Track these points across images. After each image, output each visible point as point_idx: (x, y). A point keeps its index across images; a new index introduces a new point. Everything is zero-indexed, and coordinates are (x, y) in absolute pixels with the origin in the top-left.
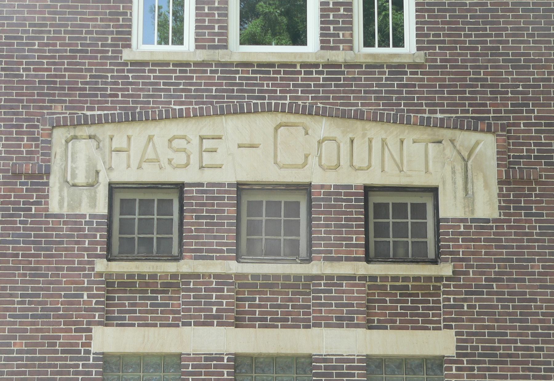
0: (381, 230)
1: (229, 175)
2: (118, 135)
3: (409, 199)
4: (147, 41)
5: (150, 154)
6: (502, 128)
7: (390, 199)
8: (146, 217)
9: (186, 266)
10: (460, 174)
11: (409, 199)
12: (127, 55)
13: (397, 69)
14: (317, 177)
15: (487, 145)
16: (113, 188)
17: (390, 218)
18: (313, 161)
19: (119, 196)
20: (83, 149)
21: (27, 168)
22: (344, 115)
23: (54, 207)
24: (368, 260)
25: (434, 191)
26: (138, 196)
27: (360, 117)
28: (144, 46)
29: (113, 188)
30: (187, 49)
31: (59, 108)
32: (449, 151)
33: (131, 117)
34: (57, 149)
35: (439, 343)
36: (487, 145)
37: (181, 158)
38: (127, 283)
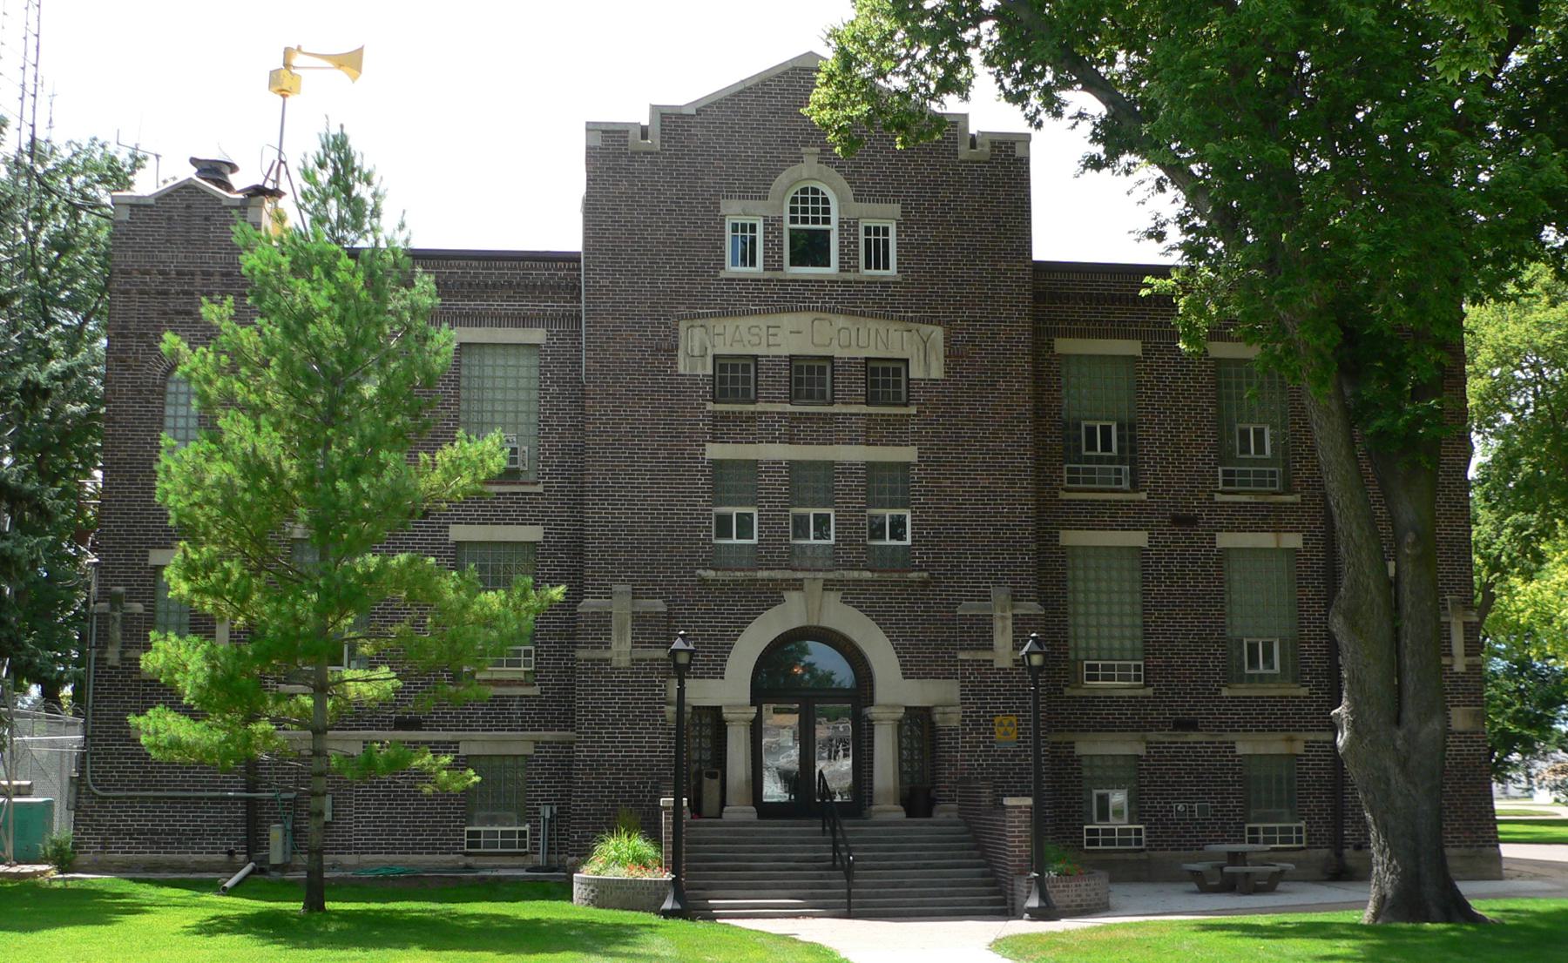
0: (875, 383)
1: (785, 351)
2: (718, 325)
3: (891, 365)
4: (734, 264)
5: (737, 337)
6: (948, 324)
7: (880, 365)
8: (734, 375)
9: (760, 407)
10: (921, 351)
11: (891, 365)
12: (722, 274)
13: (885, 284)
14: (837, 352)
15: (938, 333)
16: (715, 357)
17: (882, 378)
18: (835, 342)
19: (718, 362)
20: (698, 333)
21: (665, 345)
22: (853, 313)
23: (681, 370)
24: (867, 404)
25: (906, 361)
26: (730, 362)
27: (863, 314)
28: (733, 270)
29: (715, 357)
30: (759, 269)
31: (682, 308)
32: (916, 337)
33: (725, 314)
34: (682, 334)
35: (908, 454)
36: (938, 333)
37: (755, 340)
38: (725, 417)
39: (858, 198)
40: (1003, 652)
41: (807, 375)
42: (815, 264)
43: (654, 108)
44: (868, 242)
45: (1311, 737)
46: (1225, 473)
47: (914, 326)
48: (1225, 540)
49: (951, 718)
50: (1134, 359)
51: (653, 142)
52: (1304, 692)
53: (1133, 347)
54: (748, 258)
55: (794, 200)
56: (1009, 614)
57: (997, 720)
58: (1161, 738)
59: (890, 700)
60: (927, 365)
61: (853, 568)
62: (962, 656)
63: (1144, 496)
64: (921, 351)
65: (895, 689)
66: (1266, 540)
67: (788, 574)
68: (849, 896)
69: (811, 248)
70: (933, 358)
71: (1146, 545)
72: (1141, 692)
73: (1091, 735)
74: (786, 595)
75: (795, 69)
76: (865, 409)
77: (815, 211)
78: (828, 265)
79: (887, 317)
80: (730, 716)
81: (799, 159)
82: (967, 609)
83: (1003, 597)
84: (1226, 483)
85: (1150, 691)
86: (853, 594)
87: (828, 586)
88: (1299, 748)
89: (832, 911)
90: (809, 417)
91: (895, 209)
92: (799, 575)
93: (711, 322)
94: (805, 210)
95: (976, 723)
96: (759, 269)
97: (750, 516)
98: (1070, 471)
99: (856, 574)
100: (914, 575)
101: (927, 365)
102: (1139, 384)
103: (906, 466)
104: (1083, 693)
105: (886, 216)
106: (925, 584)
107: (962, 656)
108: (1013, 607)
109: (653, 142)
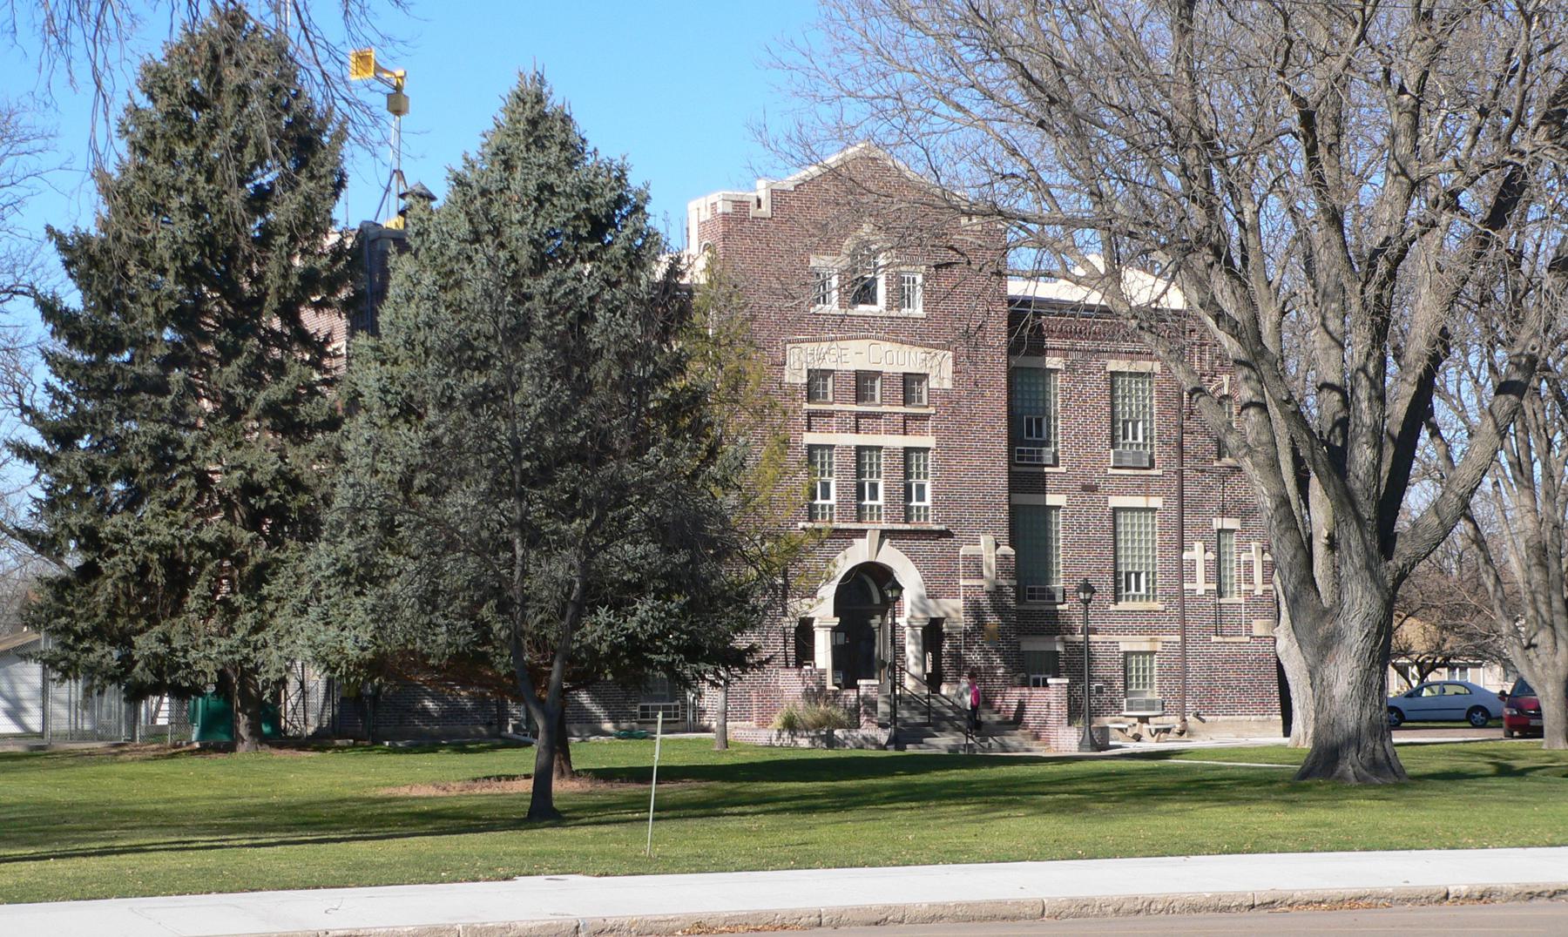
1: (852, 367)
45: (1167, 638)
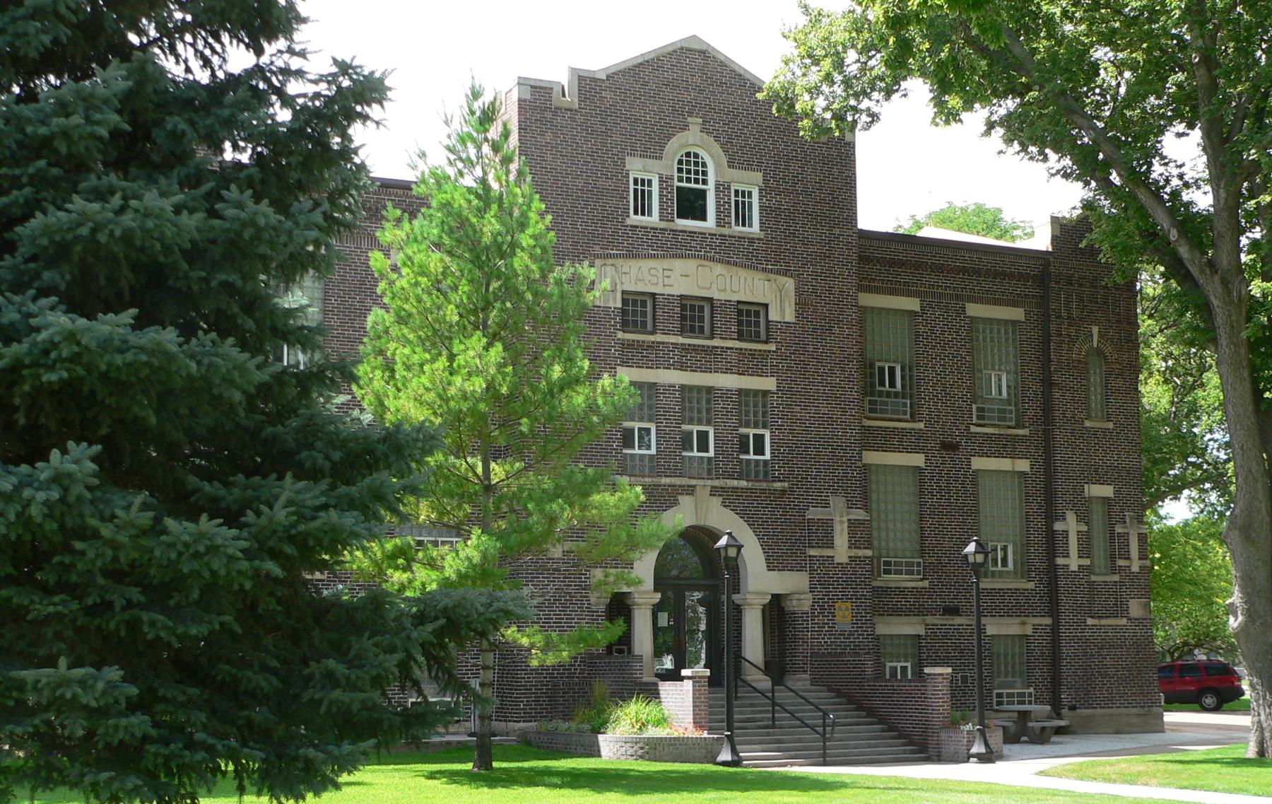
1: (676, 291)
6: (797, 277)
10: (777, 296)
13: (752, 240)
15: (790, 284)
16: (623, 292)
17: (748, 317)
22: (728, 263)
24: (682, 332)
25: (766, 306)
27: (735, 264)
29: (623, 292)
31: (597, 248)
32: (774, 286)
33: (631, 255)
35: (769, 383)
36: (790, 284)
37: (654, 280)
39: (731, 165)
40: (841, 550)
41: (692, 313)
42: (695, 218)
43: (573, 70)
44: (636, 191)
45: (1037, 621)
46: (979, 409)
47: (773, 276)
48: (978, 463)
49: (803, 604)
50: (912, 313)
51: (571, 99)
52: (1031, 585)
53: (913, 304)
54: (643, 209)
55: (680, 162)
56: (845, 519)
57: (837, 605)
58: (936, 622)
59: (759, 588)
60: (783, 311)
61: (731, 477)
62: (813, 552)
63: (922, 425)
64: (777, 296)
65: (760, 579)
66: (1004, 464)
67: (677, 481)
68: (824, 748)
69: (691, 204)
70: (787, 304)
71: (923, 465)
72: (920, 584)
73: (886, 619)
74: (680, 498)
75: (682, 48)
76: (738, 344)
77: (697, 173)
78: (704, 218)
79: (753, 268)
80: (640, 601)
81: (685, 127)
82: (814, 513)
83: (841, 505)
84: (979, 417)
85: (926, 584)
86: (730, 499)
87: (714, 491)
88: (1029, 631)
89: (808, 761)
90: (695, 348)
91: (758, 177)
92: (693, 482)
93: (620, 262)
94: (689, 172)
95: (822, 607)
96: (710, 223)
97: (707, 432)
98: (871, 402)
99: (735, 483)
100: (778, 485)
101: (783, 311)
102: (917, 334)
103: (765, 393)
104: (881, 584)
105: (750, 182)
106: (783, 492)
107: (813, 552)
108: (848, 513)
109: (571, 99)
